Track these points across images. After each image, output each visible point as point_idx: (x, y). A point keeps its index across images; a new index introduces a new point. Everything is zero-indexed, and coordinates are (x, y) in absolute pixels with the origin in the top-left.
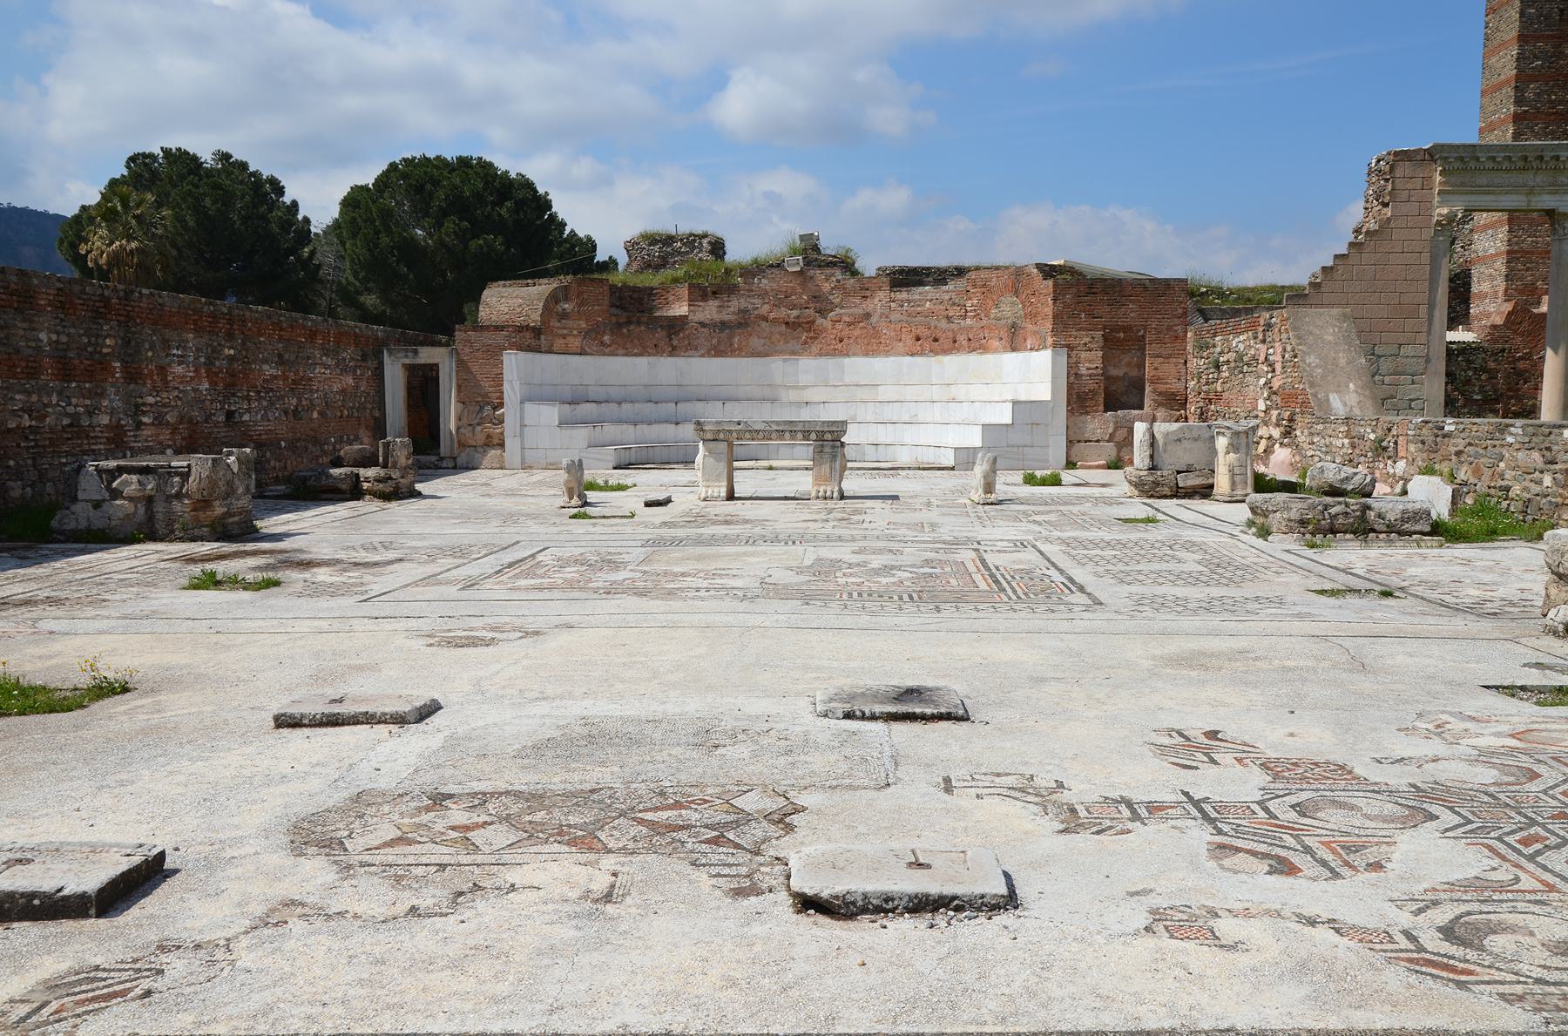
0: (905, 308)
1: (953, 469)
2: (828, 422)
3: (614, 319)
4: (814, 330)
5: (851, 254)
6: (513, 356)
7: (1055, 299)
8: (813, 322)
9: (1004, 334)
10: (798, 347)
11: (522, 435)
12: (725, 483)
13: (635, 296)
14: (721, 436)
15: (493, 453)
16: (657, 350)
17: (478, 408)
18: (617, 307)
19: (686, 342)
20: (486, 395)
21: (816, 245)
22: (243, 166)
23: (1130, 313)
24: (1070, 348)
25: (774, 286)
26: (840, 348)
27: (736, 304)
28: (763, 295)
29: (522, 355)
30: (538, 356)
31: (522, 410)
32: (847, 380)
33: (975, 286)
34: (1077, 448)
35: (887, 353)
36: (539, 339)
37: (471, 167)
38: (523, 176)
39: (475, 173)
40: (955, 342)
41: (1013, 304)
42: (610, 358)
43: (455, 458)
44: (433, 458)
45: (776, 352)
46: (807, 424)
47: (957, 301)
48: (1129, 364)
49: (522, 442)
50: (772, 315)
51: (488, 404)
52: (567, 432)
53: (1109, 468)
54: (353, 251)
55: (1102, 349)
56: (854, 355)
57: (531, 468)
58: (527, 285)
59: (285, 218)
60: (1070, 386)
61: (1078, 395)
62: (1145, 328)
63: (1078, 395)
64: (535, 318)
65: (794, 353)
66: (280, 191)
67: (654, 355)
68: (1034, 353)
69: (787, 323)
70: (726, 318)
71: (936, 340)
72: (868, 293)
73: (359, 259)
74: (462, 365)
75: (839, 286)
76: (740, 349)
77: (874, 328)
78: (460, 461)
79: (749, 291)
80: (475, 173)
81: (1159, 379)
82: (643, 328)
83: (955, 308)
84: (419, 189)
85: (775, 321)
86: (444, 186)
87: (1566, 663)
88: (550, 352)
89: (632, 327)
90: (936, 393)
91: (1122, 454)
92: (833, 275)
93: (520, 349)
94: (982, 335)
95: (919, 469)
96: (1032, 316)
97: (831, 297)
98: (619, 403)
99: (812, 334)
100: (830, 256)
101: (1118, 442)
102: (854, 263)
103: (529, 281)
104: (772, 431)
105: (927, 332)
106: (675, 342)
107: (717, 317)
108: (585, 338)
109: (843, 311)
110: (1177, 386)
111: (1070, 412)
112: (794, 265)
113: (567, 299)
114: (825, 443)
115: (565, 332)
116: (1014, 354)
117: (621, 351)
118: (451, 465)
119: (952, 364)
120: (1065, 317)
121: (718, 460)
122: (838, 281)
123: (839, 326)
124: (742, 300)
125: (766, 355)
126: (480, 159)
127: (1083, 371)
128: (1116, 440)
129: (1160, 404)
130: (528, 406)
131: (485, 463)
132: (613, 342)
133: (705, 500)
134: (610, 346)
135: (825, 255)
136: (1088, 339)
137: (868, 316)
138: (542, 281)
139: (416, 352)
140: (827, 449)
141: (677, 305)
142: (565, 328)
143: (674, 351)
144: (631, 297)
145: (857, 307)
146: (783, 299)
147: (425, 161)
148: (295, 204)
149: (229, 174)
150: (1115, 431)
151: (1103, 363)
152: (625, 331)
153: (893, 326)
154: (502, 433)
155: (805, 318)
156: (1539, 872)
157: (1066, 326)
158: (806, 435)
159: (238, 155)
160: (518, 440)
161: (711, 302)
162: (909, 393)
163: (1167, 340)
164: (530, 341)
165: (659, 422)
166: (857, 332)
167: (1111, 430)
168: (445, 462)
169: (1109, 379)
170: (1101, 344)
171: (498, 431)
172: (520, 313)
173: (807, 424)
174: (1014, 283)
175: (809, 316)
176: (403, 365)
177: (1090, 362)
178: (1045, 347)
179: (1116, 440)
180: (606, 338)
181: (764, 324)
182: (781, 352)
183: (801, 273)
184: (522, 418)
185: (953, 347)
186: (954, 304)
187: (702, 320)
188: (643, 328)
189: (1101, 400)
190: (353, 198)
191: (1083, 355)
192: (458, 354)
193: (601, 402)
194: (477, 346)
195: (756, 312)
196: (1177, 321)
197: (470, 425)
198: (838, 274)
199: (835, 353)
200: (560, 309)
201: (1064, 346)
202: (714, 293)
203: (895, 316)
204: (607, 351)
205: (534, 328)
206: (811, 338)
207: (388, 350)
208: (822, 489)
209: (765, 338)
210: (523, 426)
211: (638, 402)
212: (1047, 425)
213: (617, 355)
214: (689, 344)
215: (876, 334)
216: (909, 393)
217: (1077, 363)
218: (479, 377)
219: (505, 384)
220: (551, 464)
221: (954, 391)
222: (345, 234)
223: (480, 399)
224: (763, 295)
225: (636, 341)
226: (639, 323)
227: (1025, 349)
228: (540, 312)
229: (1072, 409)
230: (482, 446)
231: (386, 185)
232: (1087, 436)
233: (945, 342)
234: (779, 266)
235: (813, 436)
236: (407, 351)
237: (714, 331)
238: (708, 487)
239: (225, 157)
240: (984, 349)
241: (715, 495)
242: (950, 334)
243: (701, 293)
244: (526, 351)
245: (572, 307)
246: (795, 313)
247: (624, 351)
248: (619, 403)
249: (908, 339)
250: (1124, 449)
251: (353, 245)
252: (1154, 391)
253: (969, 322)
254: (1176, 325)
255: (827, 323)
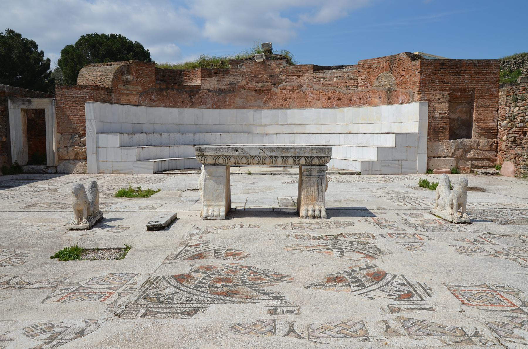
0: (322, 82)
1: (360, 173)
2: (317, 149)
3: (158, 86)
4: (271, 94)
5: (289, 55)
6: (91, 105)
7: (421, 72)
8: (270, 90)
9: (383, 95)
10: (262, 104)
11: (97, 153)
12: (224, 203)
13: (172, 75)
14: (221, 161)
15: (80, 164)
16: (183, 104)
17: (70, 136)
18: (161, 80)
19: (200, 100)
20: (75, 129)
21: (271, 50)
22: (19, 36)
23: (466, 81)
24: (430, 101)
25: (249, 70)
26: (285, 104)
27: (228, 79)
28: (243, 75)
29: (97, 104)
30: (109, 106)
31: (97, 138)
32: (289, 122)
33: (363, 68)
34: (433, 161)
35: (311, 107)
36: (111, 96)
37: (116, 38)
38: (138, 43)
39: (118, 40)
40: (351, 100)
41: (389, 77)
42: (156, 108)
43: (56, 167)
44: (42, 167)
45: (249, 106)
46: (297, 151)
47: (352, 77)
48: (461, 112)
49: (98, 157)
50: (247, 86)
51: (77, 134)
52: (125, 152)
53: (452, 173)
54: (66, 72)
55: (449, 102)
56: (293, 108)
57: (103, 173)
58: (107, 65)
59: (37, 58)
60: (430, 124)
61: (434, 130)
62: (474, 89)
63: (434, 130)
64: (108, 83)
65: (259, 107)
66: (36, 47)
67: (182, 107)
68: (404, 105)
69: (256, 91)
70: (222, 87)
71: (339, 99)
72: (301, 74)
73: (69, 75)
74: (60, 110)
75: (284, 70)
76: (230, 104)
77: (304, 93)
78: (59, 169)
79: (235, 72)
80: (118, 40)
81: (482, 120)
82: (175, 92)
83: (351, 81)
84: (94, 46)
85: (249, 89)
86: (104, 45)
87: (520, 229)
88: (118, 103)
89: (169, 91)
90: (339, 129)
91: (459, 165)
92: (281, 64)
93: (97, 100)
94: (368, 96)
95: (340, 174)
96: (403, 84)
97: (280, 76)
98: (161, 134)
99: (269, 97)
100: (278, 55)
101: (457, 158)
102: (291, 60)
103: (108, 63)
104: (266, 157)
105: (334, 95)
106: (193, 100)
107: (217, 87)
108: (140, 96)
109: (287, 84)
110: (492, 124)
111: (429, 140)
112: (260, 58)
113: (129, 73)
114: (313, 167)
115: (128, 92)
116: (390, 106)
117: (162, 104)
118: (54, 171)
119: (349, 112)
120: (427, 83)
121: (218, 183)
122: (284, 67)
123: (285, 92)
124: (231, 78)
125: (244, 108)
126: (120, 35)
127: (437, 115)
128: (456, 156)
129: (482, 135)
130: (101, 136)
131: (75, 170)
132: (158, 99)
133: (206, 219)
134: (156, 101)
135: (275, 55)
136: (440, 96)
137: (300, 86)
138: (115, 63)
139: (30, 102)
140: (315, 173)
141: (195, 80)
142: (128, 90)
143: (193, 105)
144: (169, 75)
145: (295, 82)
146: (254, 77)
147: (97, 35)
148: (42, 52)
149: (12, 38)
150: (456, 150)
151: (449, 110)
152: (165, 93)
153: (315, 92)
154: (85, 152)
155: (266, 87)
156: (212, 249)
157: (428, 88)
158: (296, 160)
159: (17, 31)
160: (95, 156)
161: (214, 78)
162: (324, 129)
163: (487, 97)
164: (104, 96)
165: (184, 145)
166: (294, 95)
167: (453, 151)
168: (50, 169)
169: (452, 120)
170: (448, 99)
171: (83, 150)
172: (100, 80)
173: (297, 151)
174: (389, 66)
175: (268, 86)
176: (22, 109)
177: (441, 109)
178: (413, 101)
179: (456, 156)
180: (154, 97)
181: (243, 91)
182: (253, 107)
183: (263, 63)
184: (97, 142)
185: (350, 103)
186: (350, 79)
187: (209, 88)
188: (175, 92)
189: (448, 133)
190: (66, 50)
191: (437, 105)
192: (57, 103)
193: (149, 133)
194: (69, 98)
195: (239, 84)
196: (493, 85)
197: (66, 147)
198: (284, 64)
199: (282, 107)
200: (125, 79)
201: (425, 100)
202: (216, 73)
203: (316, 86)
204: (154, 104)
205: (107, 89)
206: (269, 98)
207: (11, 100)
208: (317, 208)
209: (244, 98)
210: (98, 147)
211: (172, 133)
212: (415, 147)
213: (160, 107)
214: (202, 101)
215: (305, 96)
216: (324, 129)
217: (434, 110)
218: (71, 117)
219: (86, 121)
220: (115, 171)
221: (350, 128)
222: (63, 65)
223: (71, 131)
224: (243, 75)
225: (171, 99)
226: (173, 89)
227: (398, 103)
228: (111, 79)
229: (430, 138)
230: (73, 160)
231: (80, 45)
232: (439, 154)
233: (345, 100)
234: (252, 59)
235: (303, 161)
236: (23, 100)
237: (216, 94)
238: (209, 206)
239: (11, 32)
240: (370, 104)
241: (216, 214)
242: (348, 96)
243: (208, 73)
244: (101, 102)
245: (132, 78)
246: (260, 85)
247: (164, 105)
248: (161, 134)
249: (324, 99)
250: (460, 162)
251: (66, 69)
252: (479, 127)
253: (359, 88)
254: (492, 88)
255: (278, 91)
